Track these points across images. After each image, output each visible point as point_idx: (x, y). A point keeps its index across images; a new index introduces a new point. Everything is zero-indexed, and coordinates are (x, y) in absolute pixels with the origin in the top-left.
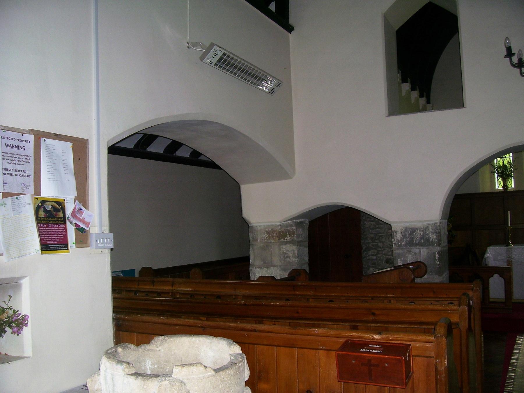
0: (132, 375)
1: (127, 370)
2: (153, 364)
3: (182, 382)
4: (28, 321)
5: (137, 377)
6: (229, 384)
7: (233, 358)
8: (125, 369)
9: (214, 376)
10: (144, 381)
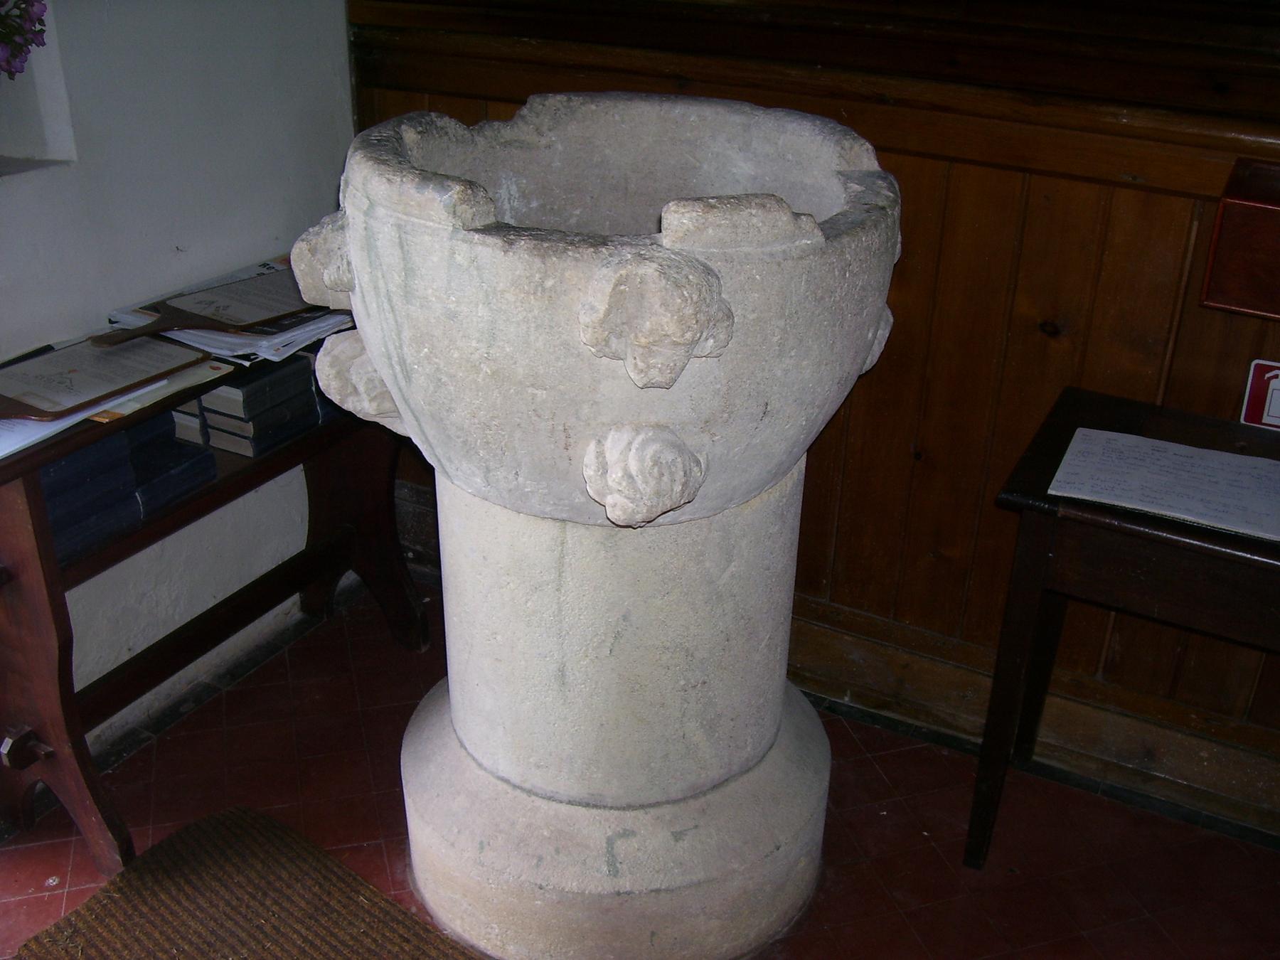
0: (486, 230)
1: (466, 211)
2: (524, 195)
3: (708, 271)
4: (42, 22)
5: (511, 243)
6: (863, 288)
7: (856, 187)
8: (460, 209)
9: (823, 252)
10: (543, 257)
